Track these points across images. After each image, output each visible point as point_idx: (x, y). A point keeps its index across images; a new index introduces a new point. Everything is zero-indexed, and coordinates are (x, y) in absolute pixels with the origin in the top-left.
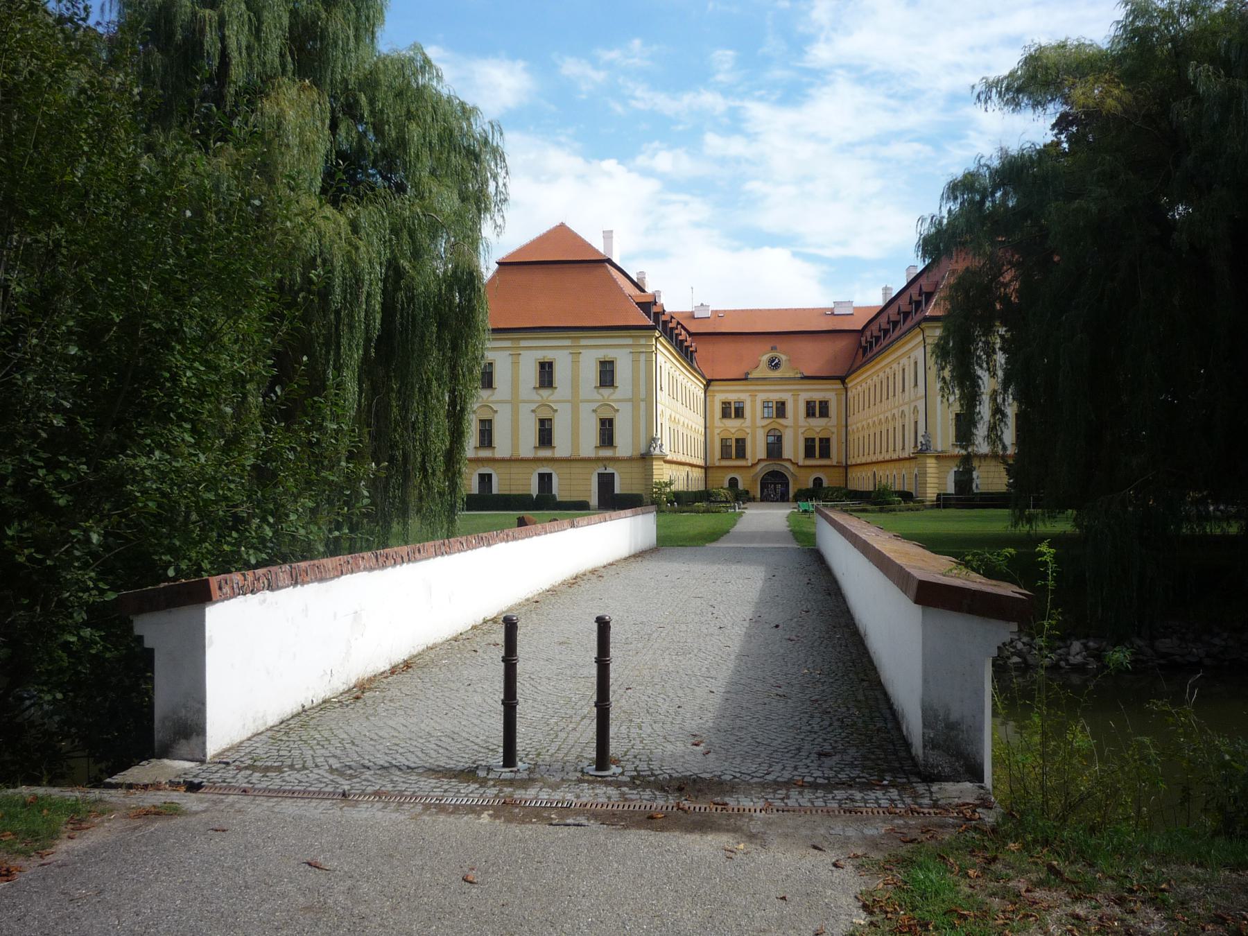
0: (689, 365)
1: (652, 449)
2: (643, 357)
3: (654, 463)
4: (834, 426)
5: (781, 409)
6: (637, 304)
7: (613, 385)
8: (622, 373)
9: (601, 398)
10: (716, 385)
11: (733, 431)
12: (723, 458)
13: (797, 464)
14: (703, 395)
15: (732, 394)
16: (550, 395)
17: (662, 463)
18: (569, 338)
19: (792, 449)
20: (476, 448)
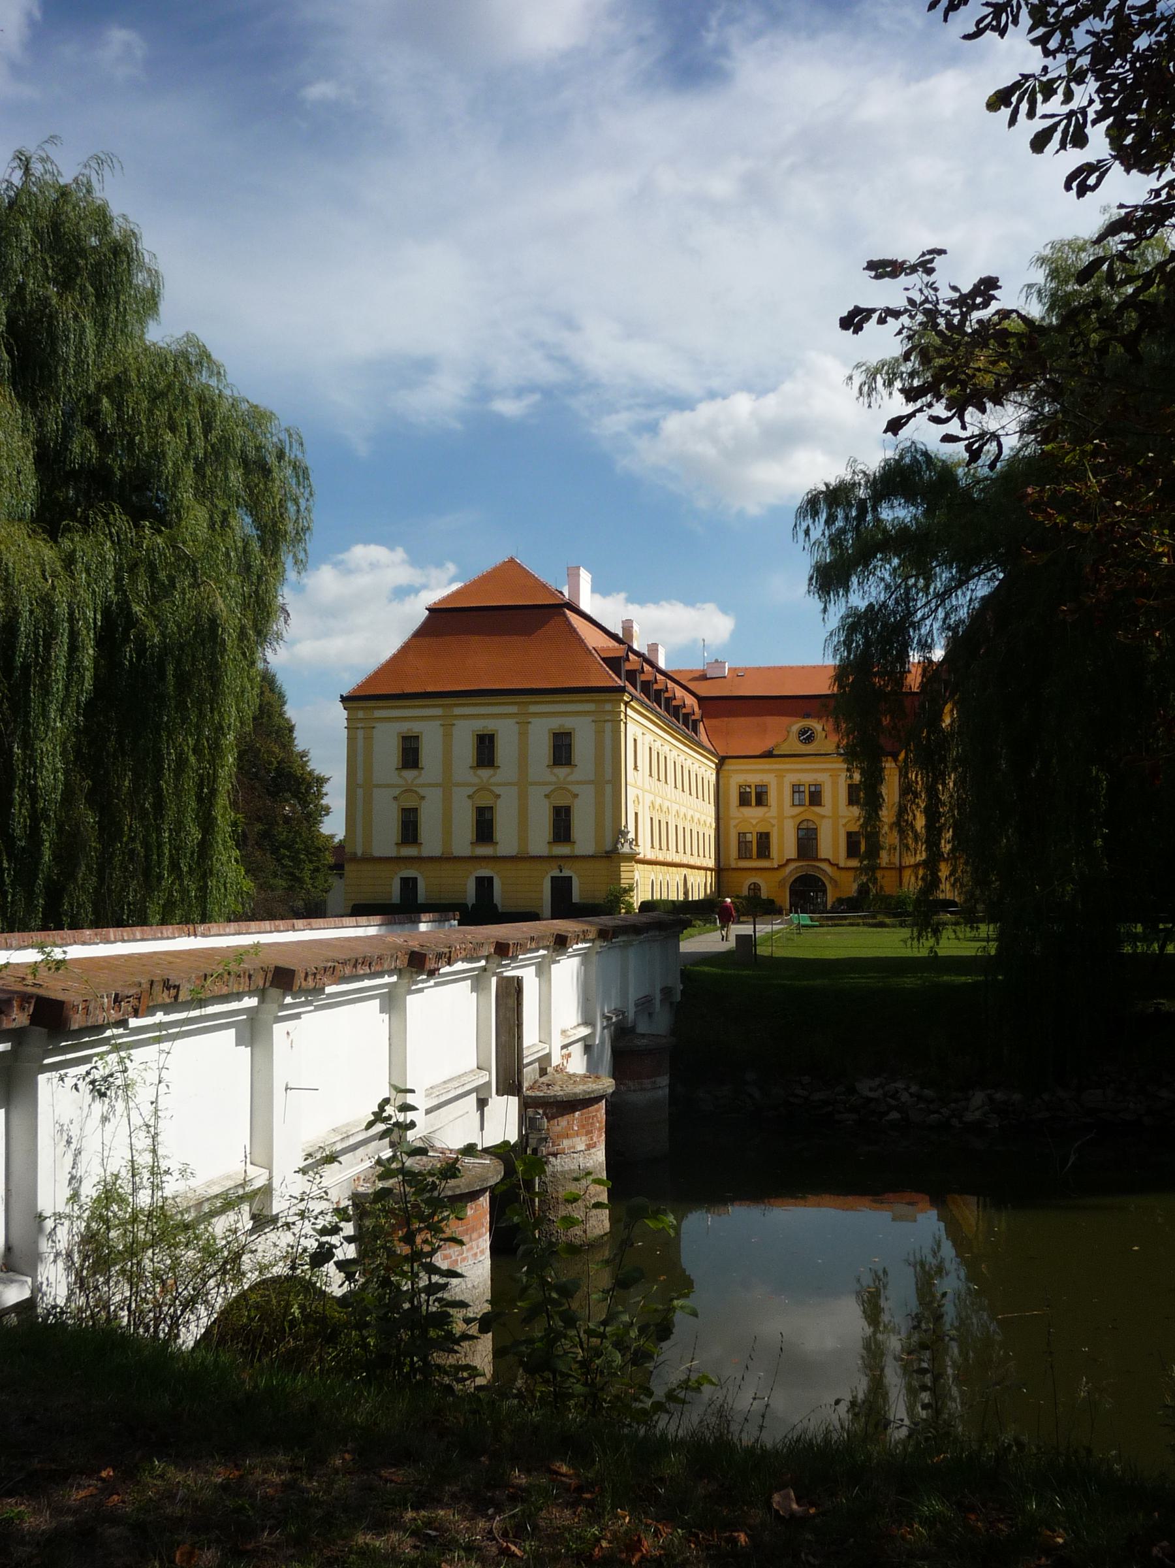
0: (686, 737)
1: (619, 846)
2: (608, 726)
4: (775, 818)
5: (815, 798)
6: (603, 659)
8: (582, 748)
11: (754, 822)
12: (740, 858)
13: (837, 865)
14: (714, 777)
16: (568, 775)
18: (515, 703)
19: (831, 845)
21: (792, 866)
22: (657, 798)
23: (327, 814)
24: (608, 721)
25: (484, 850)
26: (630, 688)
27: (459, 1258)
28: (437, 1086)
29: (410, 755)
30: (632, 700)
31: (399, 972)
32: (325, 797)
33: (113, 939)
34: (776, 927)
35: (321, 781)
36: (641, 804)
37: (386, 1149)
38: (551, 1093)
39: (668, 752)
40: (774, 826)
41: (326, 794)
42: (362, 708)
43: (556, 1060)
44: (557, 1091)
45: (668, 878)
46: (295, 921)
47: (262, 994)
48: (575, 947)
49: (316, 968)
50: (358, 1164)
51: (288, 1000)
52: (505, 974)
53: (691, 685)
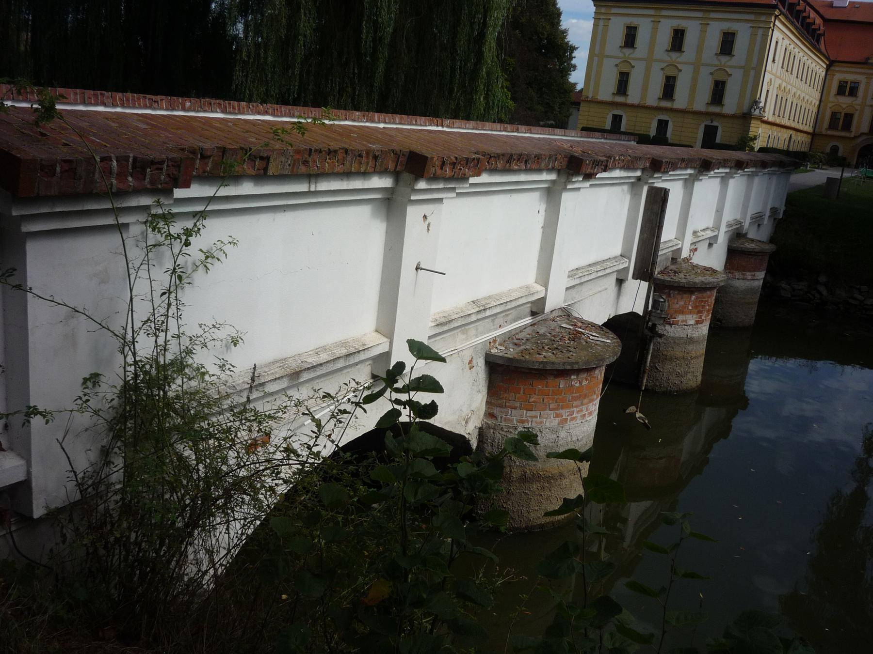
0: (812, 45)
1: (753, 110)
2: (760, 32)
3: (752, 122)
7: (681, 50)
8: (741, 44)
9: (669, 59)
10: (837, 66)
14: (824, 73)
15: (849, 76)
16: (631, 54)
17: (759, 122)
20: (659, 99)
21: (864, 137)
22: (784, 82)
23: (574, 70)
26: (781, 7)
27: (569, 418)
28: (582, 268)
29: (630, 38)
30: (780, 15)
31: (559, 172)
32: (574, 59)
33: (377, 120)
34: (847, 175)
35: (573, 49)
36: (772, 86)
37: (525, 317)
38: (676, 279)
39: (797, 53)
40: (857, 110)
41: (575, 57)
42: (605, 6)
43: (685, 254)
44: (681, 278)
45: (780, 135)
46: (520, 126)
47: (396, 175)
48: (716, 171)
49: (456, 158)
50: (496, 329)
51: (422, 185)
52: (656, 185)
53: (821, 11)
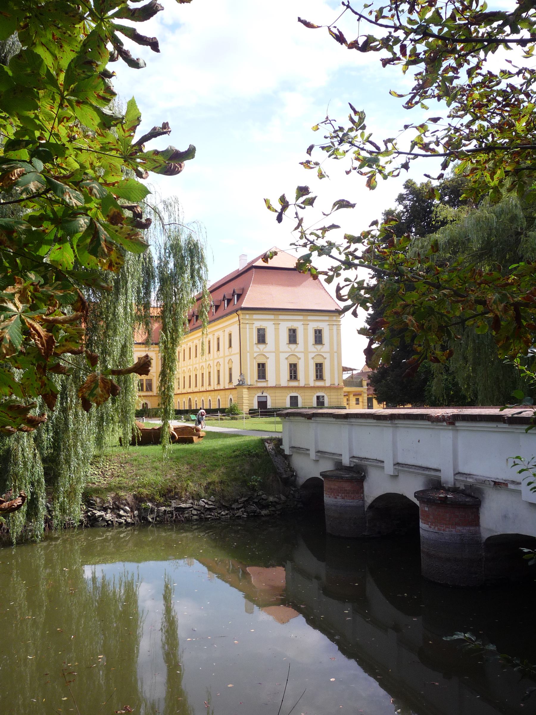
2: (335, 327)
24: (248, 323)
25: (294, 384)
29: (262, 338)
